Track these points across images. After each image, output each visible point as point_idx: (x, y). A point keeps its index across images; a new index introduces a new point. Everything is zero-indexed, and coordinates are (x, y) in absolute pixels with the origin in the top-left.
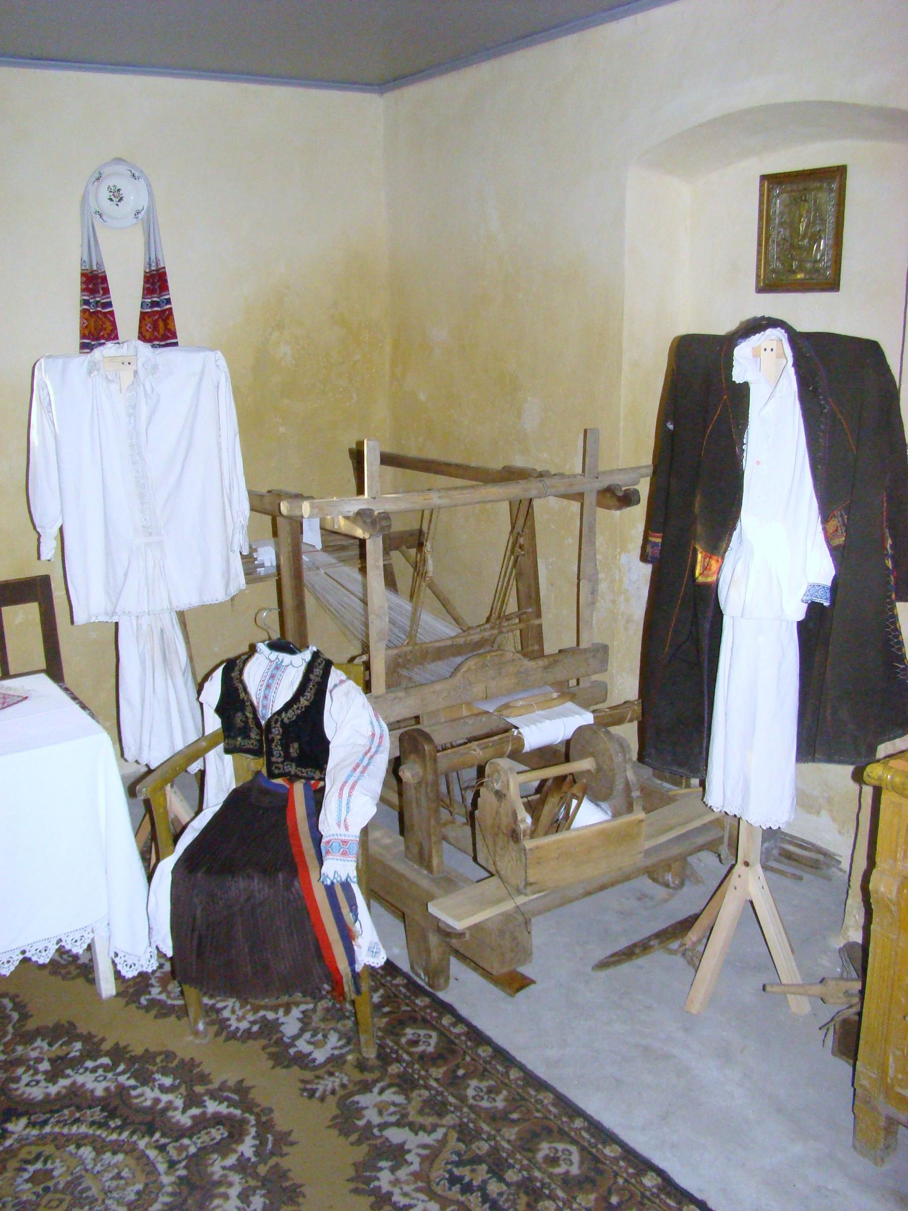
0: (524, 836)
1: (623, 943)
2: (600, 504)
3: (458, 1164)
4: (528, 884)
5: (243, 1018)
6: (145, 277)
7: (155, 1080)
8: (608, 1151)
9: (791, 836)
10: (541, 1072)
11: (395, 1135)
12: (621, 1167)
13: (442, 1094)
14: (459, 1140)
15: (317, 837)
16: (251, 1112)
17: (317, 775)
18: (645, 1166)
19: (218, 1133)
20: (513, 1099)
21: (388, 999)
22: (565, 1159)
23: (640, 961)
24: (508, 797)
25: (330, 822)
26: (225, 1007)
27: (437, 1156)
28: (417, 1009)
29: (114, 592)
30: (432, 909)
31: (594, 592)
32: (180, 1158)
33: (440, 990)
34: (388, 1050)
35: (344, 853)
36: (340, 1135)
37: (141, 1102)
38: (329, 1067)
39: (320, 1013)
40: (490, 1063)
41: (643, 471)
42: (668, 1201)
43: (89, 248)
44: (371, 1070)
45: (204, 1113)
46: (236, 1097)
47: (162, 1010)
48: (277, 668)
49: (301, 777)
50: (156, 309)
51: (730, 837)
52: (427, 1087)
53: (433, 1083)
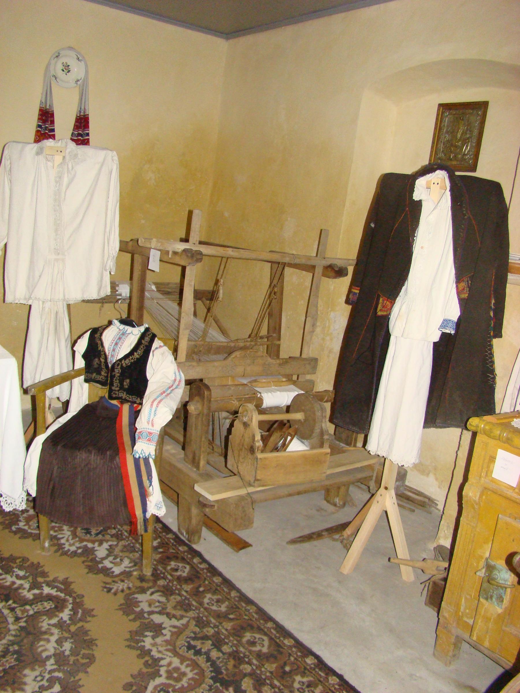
0: (257, 450)
1: (307, 532)
2: (324, 275)
3: (194, 639)
4: (256, 480)
5: (73, 544)
6: (76, 119)
7: (14, 571)
8: (286, 642)
9: (410, 488)
10: (250, 595)
11: (157, 619)
12: (293, 651)
13: (188, 599)
14: (196, 625)
15: (133, 430)
16: (71, 596)
17: (138, 401)
18: (308, 652)
19: (48, 605)
20: (232, 607)
21: (162, 545)
22: (259, 644)
23: (315, 543)
24: (251, 426)
25: (143, 421)
26: (63, 538)
27: (181, 633)
28: (179, 552)
29: (31, 287)
30: (197, 488)
31: (314, 325)
32: (22, 616)
33: (195, 543)
34: (159, 572)
35: (149, 440)
36: (123, 614)
37: (4, 583)
38: (122, 577)
39: (120, 547)
40: (220, 586)
41: (351, 262)
42: (320, 673)
43: (47, 93)
44: (147, 581)
45: (42, 593)
46: (63, 587)
47: (24, 534)
48: (123, 334)
49: (128, 401)
50: (80, 138)
51: (377, 477)
52: (179, 594)
53: (184, 593)
